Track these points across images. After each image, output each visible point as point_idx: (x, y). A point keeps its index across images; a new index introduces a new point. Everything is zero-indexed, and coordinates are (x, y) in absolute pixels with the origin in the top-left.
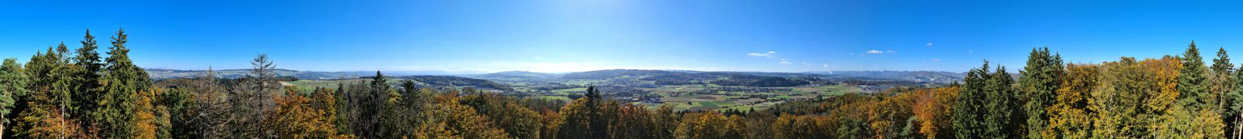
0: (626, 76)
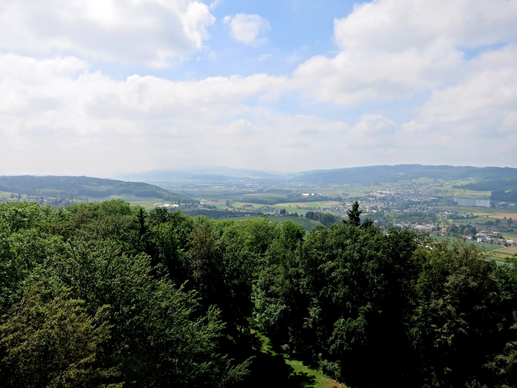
0: (422, 180)
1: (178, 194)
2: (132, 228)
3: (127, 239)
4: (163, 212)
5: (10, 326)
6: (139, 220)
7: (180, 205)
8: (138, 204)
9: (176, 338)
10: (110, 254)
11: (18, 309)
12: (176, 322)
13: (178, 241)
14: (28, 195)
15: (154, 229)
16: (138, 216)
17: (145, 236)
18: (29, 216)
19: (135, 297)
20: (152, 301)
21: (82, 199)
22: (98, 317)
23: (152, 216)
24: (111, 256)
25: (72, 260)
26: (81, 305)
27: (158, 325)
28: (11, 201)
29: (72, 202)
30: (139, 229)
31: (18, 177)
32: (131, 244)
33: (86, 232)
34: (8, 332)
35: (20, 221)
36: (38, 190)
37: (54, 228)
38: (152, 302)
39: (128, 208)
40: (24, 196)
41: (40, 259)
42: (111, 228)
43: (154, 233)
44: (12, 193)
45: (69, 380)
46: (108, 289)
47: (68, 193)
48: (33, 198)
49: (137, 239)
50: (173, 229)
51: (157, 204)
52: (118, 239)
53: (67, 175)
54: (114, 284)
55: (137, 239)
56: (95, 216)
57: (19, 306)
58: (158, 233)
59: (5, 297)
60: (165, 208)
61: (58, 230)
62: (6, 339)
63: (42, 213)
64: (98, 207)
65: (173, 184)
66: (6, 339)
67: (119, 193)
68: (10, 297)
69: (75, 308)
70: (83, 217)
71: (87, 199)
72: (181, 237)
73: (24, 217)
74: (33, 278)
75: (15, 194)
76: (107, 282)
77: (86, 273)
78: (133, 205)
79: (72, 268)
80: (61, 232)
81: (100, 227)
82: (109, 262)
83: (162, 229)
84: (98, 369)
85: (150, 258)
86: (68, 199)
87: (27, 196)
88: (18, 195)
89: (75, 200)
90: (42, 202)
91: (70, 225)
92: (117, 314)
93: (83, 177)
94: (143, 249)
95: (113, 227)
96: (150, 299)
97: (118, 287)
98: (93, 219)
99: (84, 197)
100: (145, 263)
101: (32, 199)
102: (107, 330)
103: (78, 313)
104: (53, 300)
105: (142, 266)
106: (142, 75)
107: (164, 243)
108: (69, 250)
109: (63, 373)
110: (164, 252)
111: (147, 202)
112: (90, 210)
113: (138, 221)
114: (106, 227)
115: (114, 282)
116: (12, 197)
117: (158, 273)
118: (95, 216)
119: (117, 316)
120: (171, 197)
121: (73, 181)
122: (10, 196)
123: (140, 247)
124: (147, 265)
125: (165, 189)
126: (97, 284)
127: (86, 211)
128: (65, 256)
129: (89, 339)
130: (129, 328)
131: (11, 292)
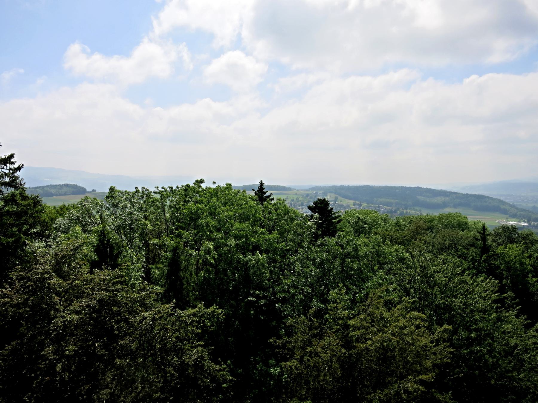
1: (528, 211)
2: (473, 245)
3: (466, 258)
4: (511, 231)
5: (357, 323)
6: (481, 237)
7: (530, 224)
8: (478, 220)
9: (526, 386)
10: (452, 271)
11: (364, 309)
12: (527, 366)
13: (529, 268)
14: (367, 204)
15: (500, 250)
16: (479, 233)
17: (487, 257)
18: (369, 223)
19: (476, 324)
20: (499, 334)
21: (416, 210)
22: (437, 336)
23: (497, 234)
24: (452, 274)
25: (412, 271)
26: (422, 320)
27: (504, 364)
28: (354, 208)
29: (407, 212)
30: (480, 248)
31: (360, 186)
32: (470, 263)
33: (422, 245)
34: (355, 327)
35: (362, 227)
36: (376, 199)
37: (392, 236)
38: (499, 335)
39: (466, 223)
40: (364, 205)
41: (381, 266)
42: (447, 243)
43: (498, 254)
44: (354, 201)
45: (406, 391)
46: (448, 308)
47: (403, 203)
48: (371, 206)
49: (478, 258)
50: (523, 252)
51: (500, 220)
52: (456, 256)
53: (403, 186)
54: (455, 305)
55: (478, 258)
56: (431, 228)
57: (365, 306)
58: (504, 255)
59: (353, 295)
60: (514, 226)
61: (395, 239)
62: (354, 333)
63: (381, 221)
64: (434, 220)
65: (522, 198)
66: (354, 333)
67: (455, 206)
68: (357, 297)
69: (416, 321)
70: (418, 228)
71: (420, 211)
72: (534, 264)
73: (366, 223)
74: (376, 282)
75: (356, 202)
76: (447, 301)
77: (425, 287)
78: (470, 220)
79: (412, 279)
80: (398, 242)
81: (437, 241)
82: (450, 280)
83: (510, 251)
84: (433, 390)
85: (498, 283)
86: (402, 209)
87: (366, 204)
88: (359, 203)
89: (409, 211)
90: (379, 210)
91: (406, 236)
92: (456, 337)
93: (418, 187)
94: (484, 271)
95: (450, 243)
96: (495, 331)
97: (459, 309)
98: (428, 232)
99: (418, 208)
100: (492, 288)
101: (370, 208)
102: (447, 353)
103: (418, 327)
104: (395, 308)
105: (487, 291)
106: (480, 74)
107: (511, 267)
108: (409, 261)
109: (401, 382)
110: (510, 278)
111: (489, 218)
112: (425, 223)
113: (479, 238)
114: (443, 242)
115: (455, 302)
116: (354, 205)
117: (507, 303)
118: (431, 228)
119: (456, 340)
120: (518, 213)
121: (408, 192)
122: (353, 204)
123: (480, 268)
124: (493, 290)
125: (511, 203)
126: (436, 300)
127: (421, 223)
128: (405, 266)
129: (427, 355)
130: (468, 356)
131: (357, 291)
